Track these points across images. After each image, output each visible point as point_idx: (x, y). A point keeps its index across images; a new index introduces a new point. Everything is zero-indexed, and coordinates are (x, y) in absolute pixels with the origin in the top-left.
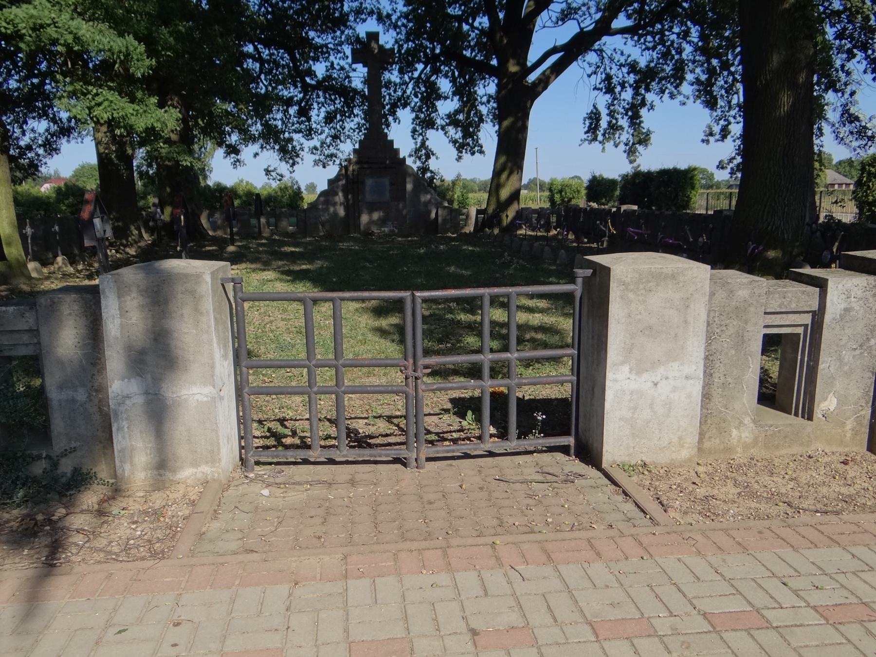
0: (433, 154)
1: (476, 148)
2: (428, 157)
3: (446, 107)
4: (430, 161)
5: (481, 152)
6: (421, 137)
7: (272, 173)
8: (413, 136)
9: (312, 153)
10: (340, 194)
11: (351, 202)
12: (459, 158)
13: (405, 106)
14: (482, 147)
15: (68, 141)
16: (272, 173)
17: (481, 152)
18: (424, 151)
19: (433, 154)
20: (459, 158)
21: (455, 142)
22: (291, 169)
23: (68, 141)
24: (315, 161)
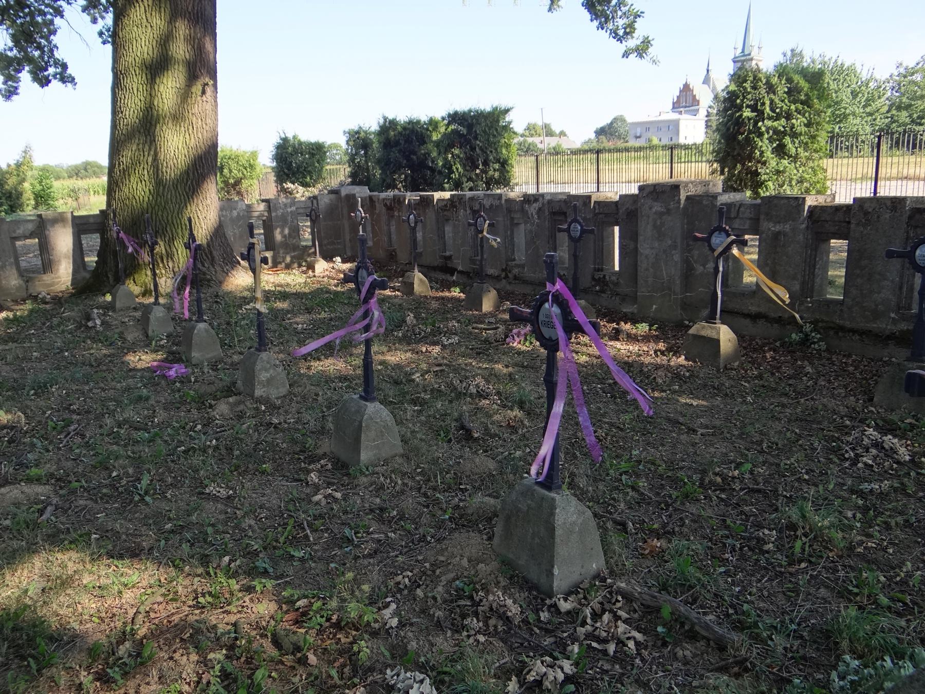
1: (51, 70)
5: (65, 78)
14: (65, 66)
17: (65, 78)
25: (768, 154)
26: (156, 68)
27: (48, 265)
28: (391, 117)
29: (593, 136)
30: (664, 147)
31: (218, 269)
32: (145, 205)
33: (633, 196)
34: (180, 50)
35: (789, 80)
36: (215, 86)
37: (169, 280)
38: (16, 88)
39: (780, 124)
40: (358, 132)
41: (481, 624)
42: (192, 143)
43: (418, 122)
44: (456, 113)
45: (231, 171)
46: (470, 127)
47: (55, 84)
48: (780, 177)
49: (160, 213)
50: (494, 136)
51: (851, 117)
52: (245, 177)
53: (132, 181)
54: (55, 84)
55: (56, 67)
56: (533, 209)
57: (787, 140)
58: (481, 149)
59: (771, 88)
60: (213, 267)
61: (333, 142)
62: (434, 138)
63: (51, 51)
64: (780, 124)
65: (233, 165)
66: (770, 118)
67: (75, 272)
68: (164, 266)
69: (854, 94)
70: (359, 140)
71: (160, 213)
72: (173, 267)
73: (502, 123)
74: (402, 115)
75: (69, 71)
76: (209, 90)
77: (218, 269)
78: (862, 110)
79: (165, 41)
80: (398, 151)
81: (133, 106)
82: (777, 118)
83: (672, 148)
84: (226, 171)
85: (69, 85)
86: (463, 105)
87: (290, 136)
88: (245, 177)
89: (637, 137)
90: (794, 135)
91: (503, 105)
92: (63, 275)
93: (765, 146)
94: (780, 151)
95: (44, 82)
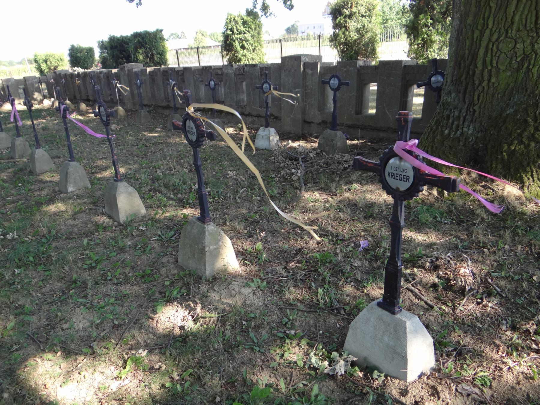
25: (239, 48)
28: (112, 35)
29: (285, 32)
30: (195, 48)
33: (277, 64)
35: (243, 19)
39: (241, 36)
40: (102, 42)
41: (226, 355)
43: (127, 36)
44: (137, 33)
45: (51, 63)
46: (143, 38)
48: (248, 58)
50: (155, 42)
51: (390, 21)
52: (59, 65)
56: (102, 75)
57: (244, 43)
58: (149, 48)
59: (236, 22)
64: (241, 36)
65: (52, 59)
66: (237, 34)
69: (391, 8)
70: (102, 46)
74: (118, 35)
78: (395, 17)
80: (119, 50)
82: (240, 33)
83: (198, 48)
84: (48, 63)
86: (140, 29)
87: (75, 45)
88: (59, 65)
89: (303, 33)
90: (247, 41)
91: (160, 28)
93: (237, 44)
94: (243, 47)
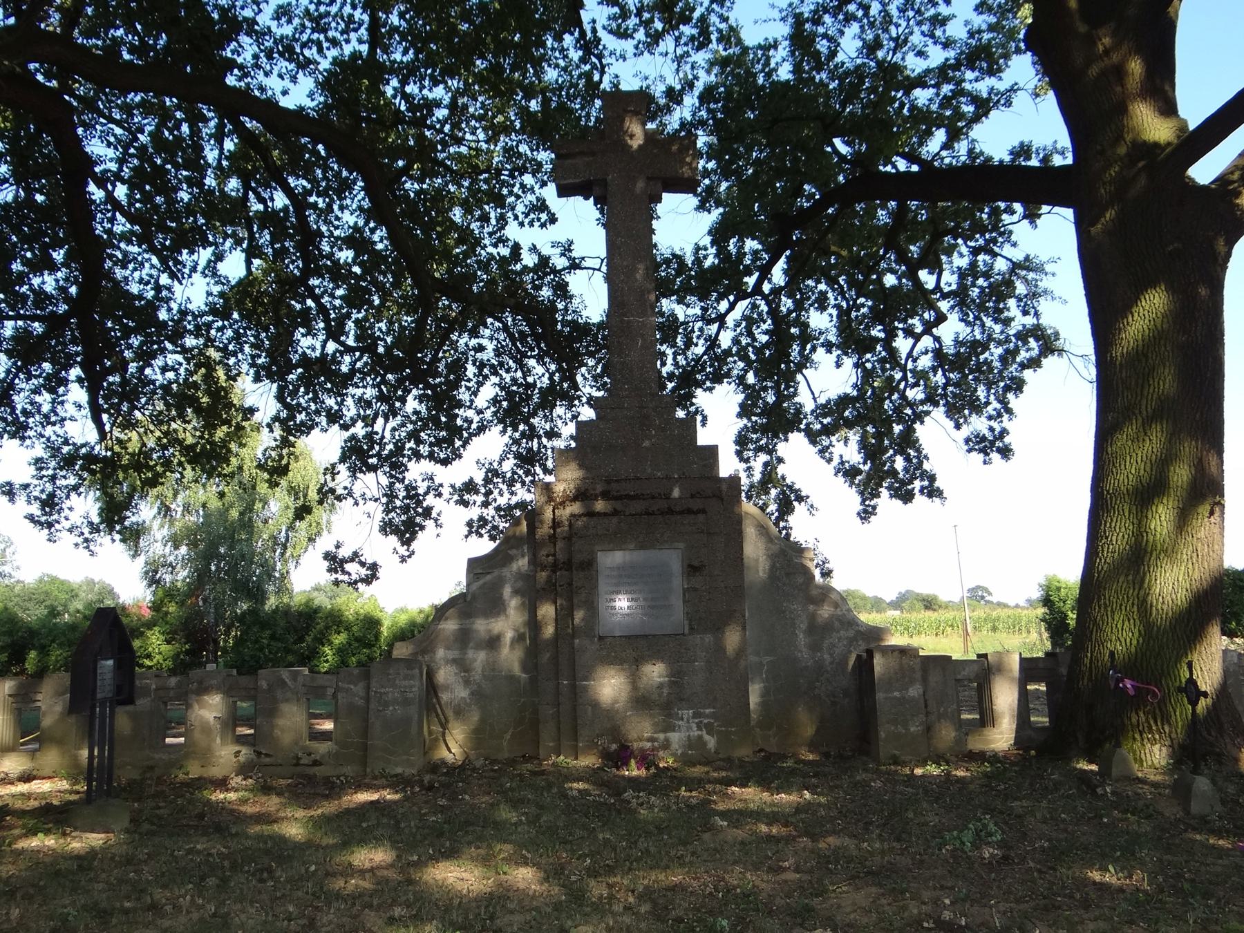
0: (800, 499)
1: (917, 484)
2: (786, 508)
3: (828, 378)
4: (792, 520)
5: (933, 492)
6: (763, 458)
7: (348, 567)
8: (739, 454)
9: (466, 504)
10: (513, 603)
11: (549, 631)
12: (866, 514)
13: (718, 378)
14: (932, 478)
15: (922, 423)
16: (348, 567)
17: (933, 492)
18: (774, 492)
19: (800, 499)
20: (866, 514)
21: (850, 473)
22: (403, 550)
23: (922, 423)
24: (470, 524)
26: (1148, 493)
27: (987, 718)
31: (1228, 740)
32: (1133, 650)
34: (1181, 474)
36: (1223, 513)
37: (1164, 749)
38: (874, 508)
42: (1196, 576)
47: (919, 499)
49: (1153, 661)
53: (1116, 618)
54: (919, 499)
55: (922, 480)
60: (1222, 736)
61: (853, 587)
62: (191, 886)
63: (921, 463)
67: (1018, 730)
68: (1158, 730)
71: (1153, 661)
72: (1170, 732)
73: (82, 787)
75: (937, 484)
76: (1217, 514)
77: (1228, 740)
79: (1163, 463)
81: (1118, 538)
85: (937, 500)
92: (1002, 736)
95: (907, 497)
